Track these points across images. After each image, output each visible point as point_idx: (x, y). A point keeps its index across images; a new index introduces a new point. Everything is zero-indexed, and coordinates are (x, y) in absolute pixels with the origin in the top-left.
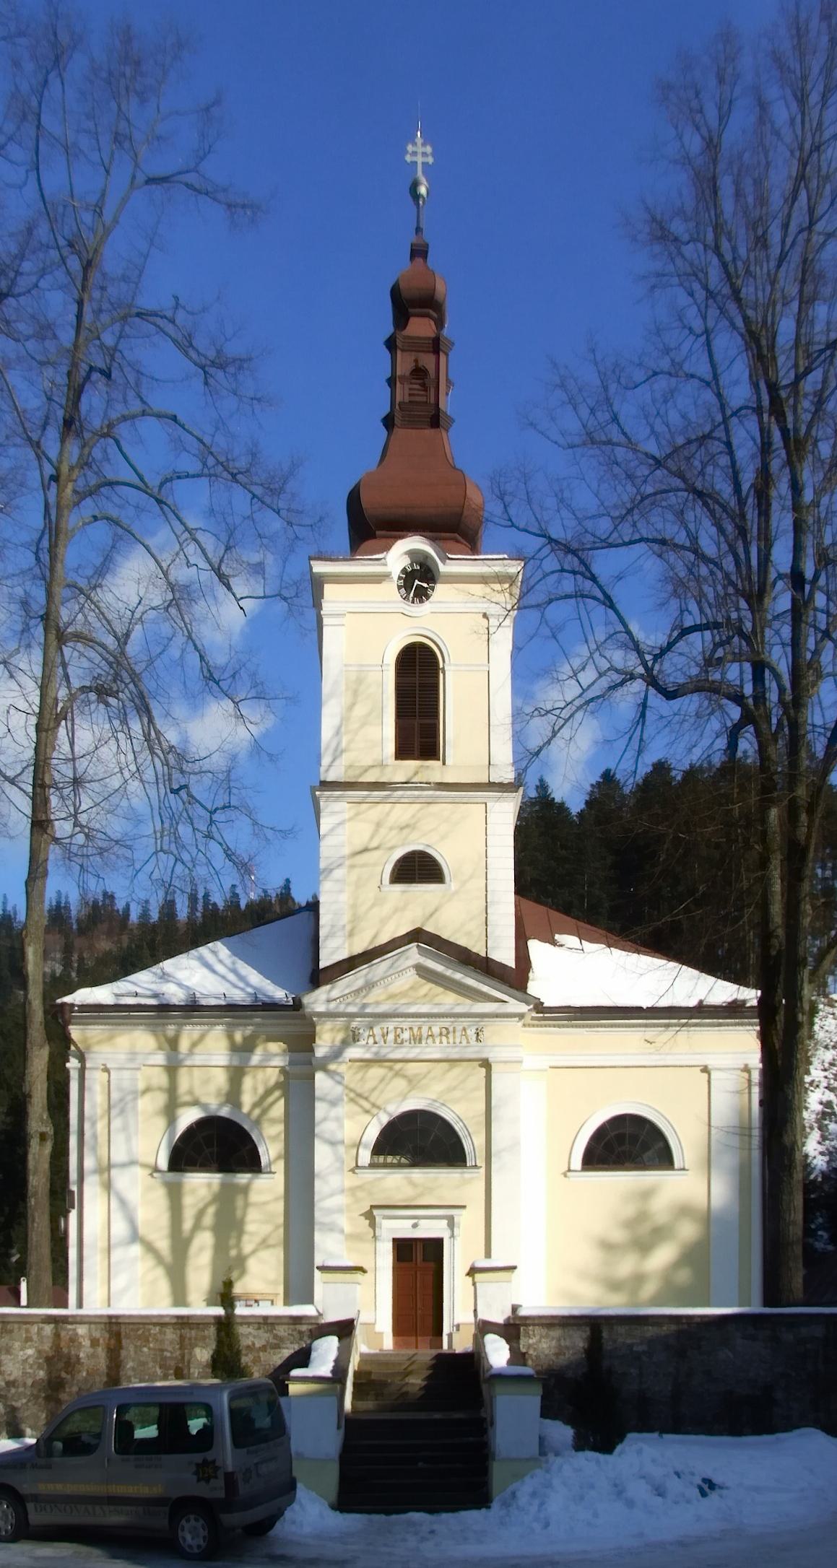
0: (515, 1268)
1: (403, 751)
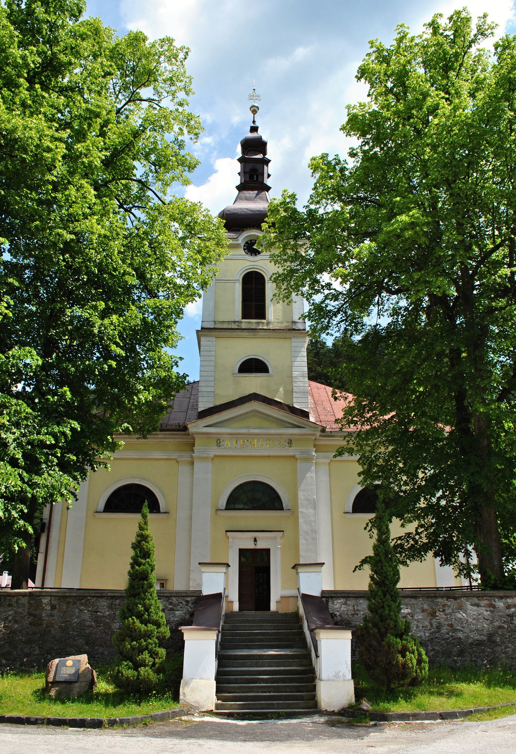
0: (324, 564)
1: (246, 315)
